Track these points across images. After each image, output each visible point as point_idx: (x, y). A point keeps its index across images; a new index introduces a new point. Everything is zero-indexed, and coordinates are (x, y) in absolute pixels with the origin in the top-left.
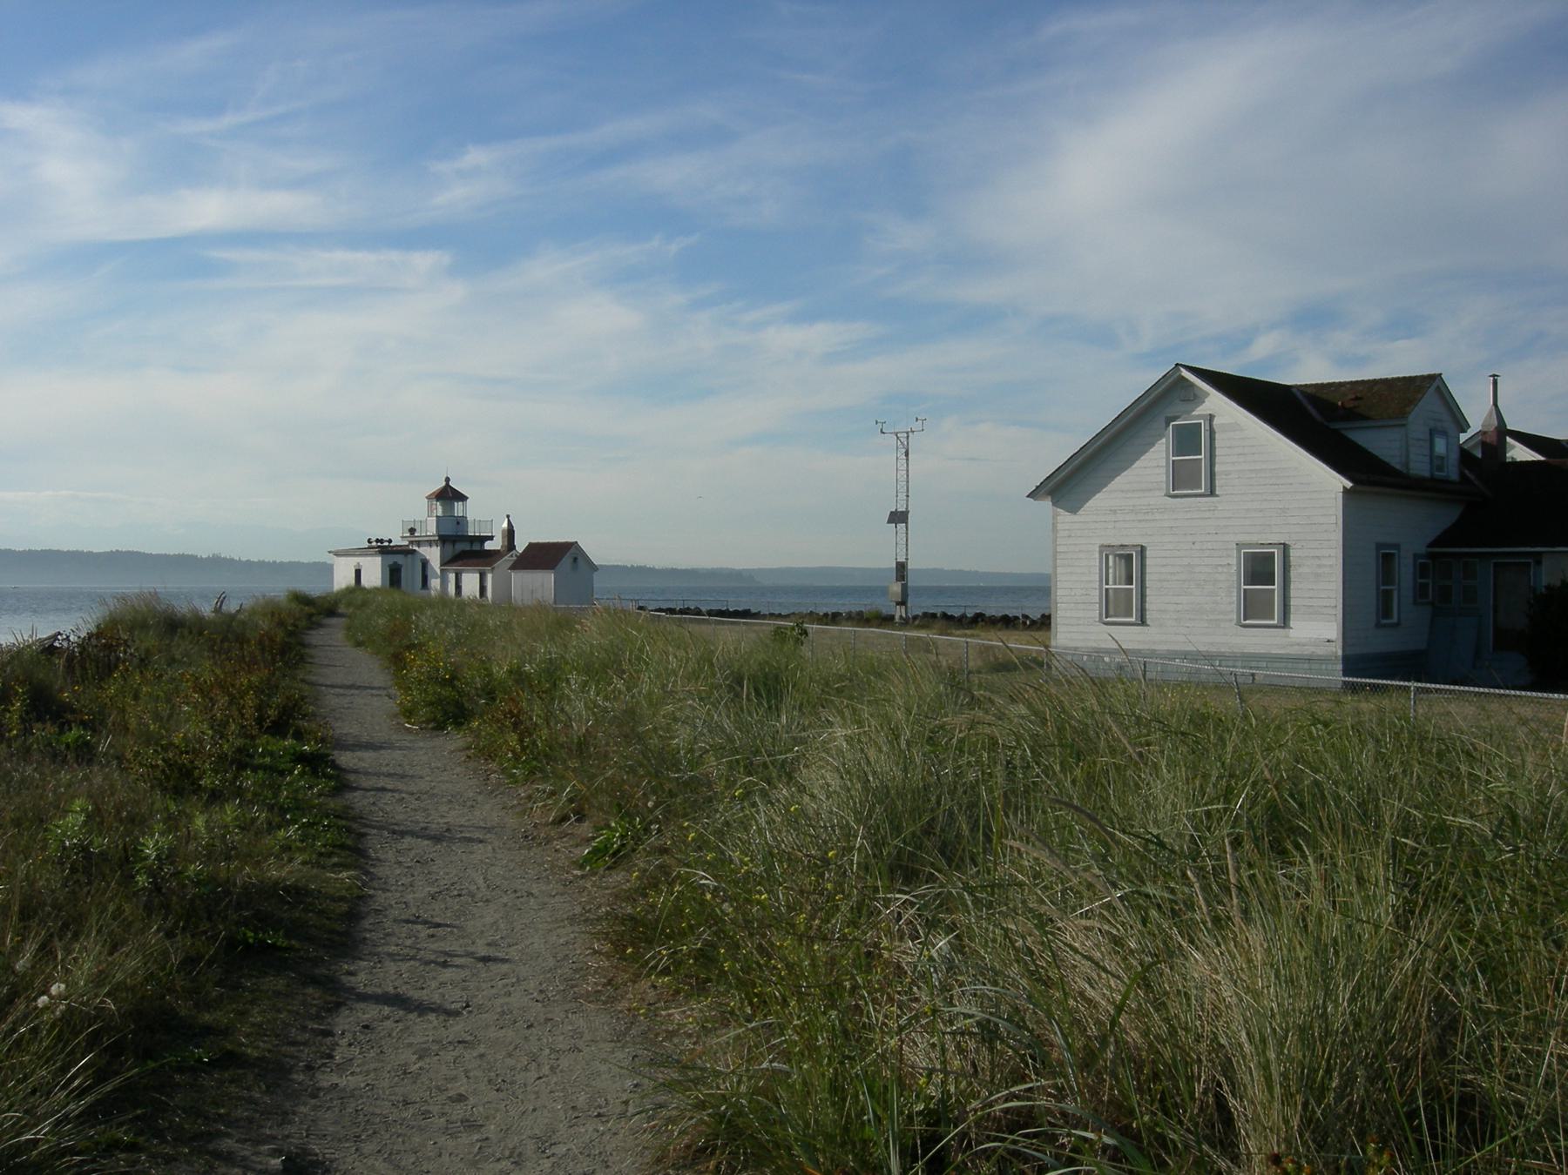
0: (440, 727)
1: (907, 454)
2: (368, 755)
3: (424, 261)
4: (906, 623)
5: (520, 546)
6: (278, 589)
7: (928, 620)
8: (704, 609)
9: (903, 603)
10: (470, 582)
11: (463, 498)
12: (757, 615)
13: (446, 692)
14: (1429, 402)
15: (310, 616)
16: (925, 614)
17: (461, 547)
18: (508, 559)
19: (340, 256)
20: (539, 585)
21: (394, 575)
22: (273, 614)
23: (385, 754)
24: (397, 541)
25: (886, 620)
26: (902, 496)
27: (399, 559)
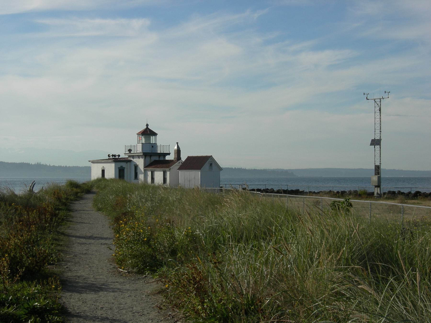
0: (141, 272)
1: (380, 110)
2: (90, 296)
3: (137, 23)
4: (380, 196)
5: (184, 158)
6: (62, 180)
7: (392, 195)
8: (275, 190)
9: (378, 186)
10: (159, 176)
11: (155, 134)
12: (302, 193)
13: (144, 248)
14: (209, 160)
15: (77, 193)
16: (389, 192)
17: (156, 158)
18: (177, 165)
19: (98, 21)
20: (192, 178)
21: (121, 173)
22: (54, 194)
23: (104, 297)
24: (123, 156)
25: (370, 195)
26: (378, 131)
27: (124, 165)
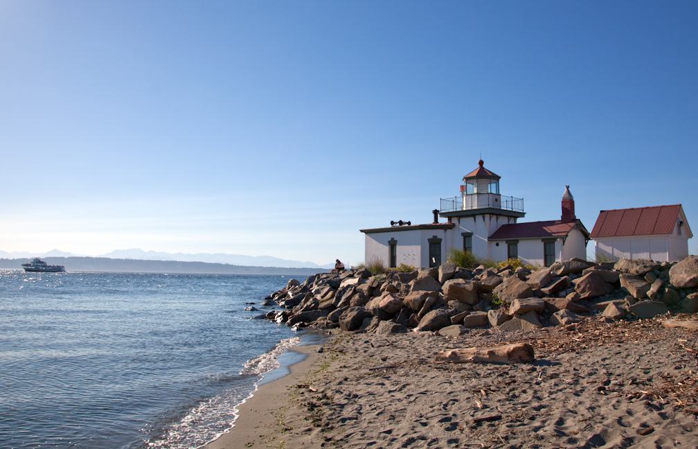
11: (496, 178)
17: (503, 221)
27: (439, 234)
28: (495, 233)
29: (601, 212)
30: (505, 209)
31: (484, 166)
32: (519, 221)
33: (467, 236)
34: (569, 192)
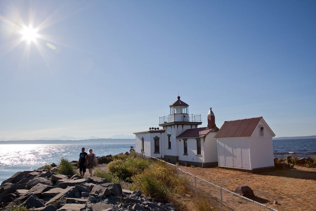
11: (186, 105)
17: (189, 127)
27: (158, 135)
28: (179, 136)
29: (225, 122)
30: (192, 121)
31: (180, 99)
32: (199, 126)
33: (169, 136)
34: (211, 112)
